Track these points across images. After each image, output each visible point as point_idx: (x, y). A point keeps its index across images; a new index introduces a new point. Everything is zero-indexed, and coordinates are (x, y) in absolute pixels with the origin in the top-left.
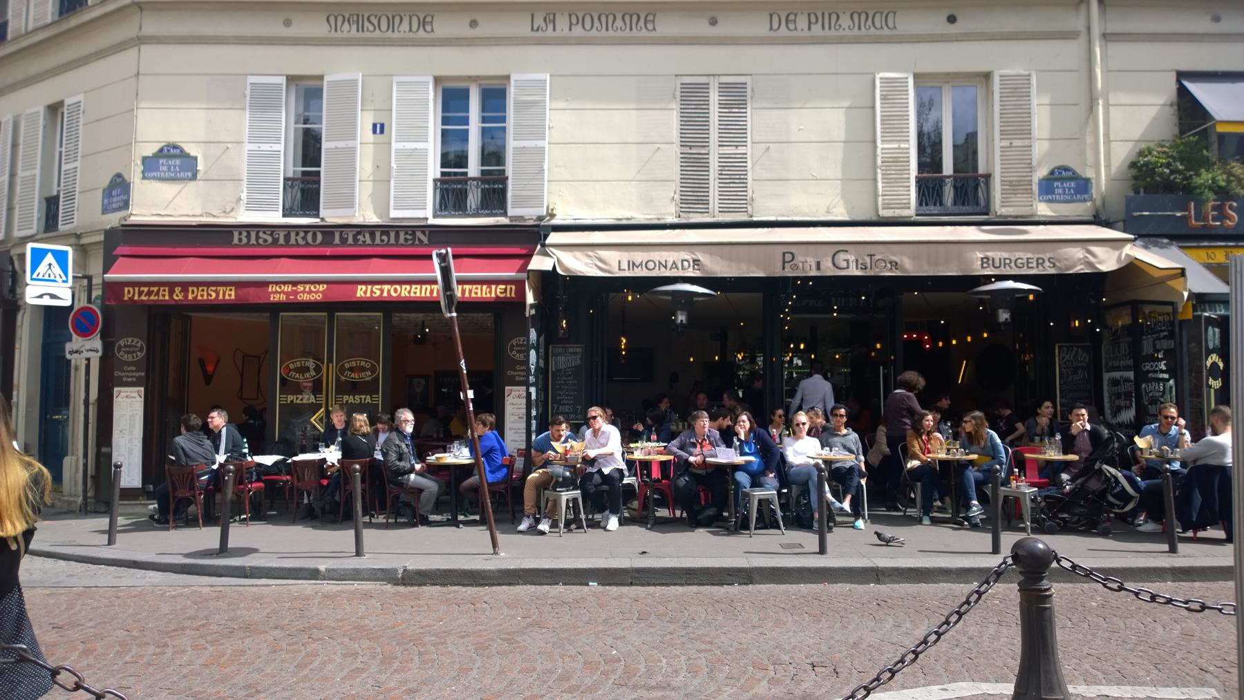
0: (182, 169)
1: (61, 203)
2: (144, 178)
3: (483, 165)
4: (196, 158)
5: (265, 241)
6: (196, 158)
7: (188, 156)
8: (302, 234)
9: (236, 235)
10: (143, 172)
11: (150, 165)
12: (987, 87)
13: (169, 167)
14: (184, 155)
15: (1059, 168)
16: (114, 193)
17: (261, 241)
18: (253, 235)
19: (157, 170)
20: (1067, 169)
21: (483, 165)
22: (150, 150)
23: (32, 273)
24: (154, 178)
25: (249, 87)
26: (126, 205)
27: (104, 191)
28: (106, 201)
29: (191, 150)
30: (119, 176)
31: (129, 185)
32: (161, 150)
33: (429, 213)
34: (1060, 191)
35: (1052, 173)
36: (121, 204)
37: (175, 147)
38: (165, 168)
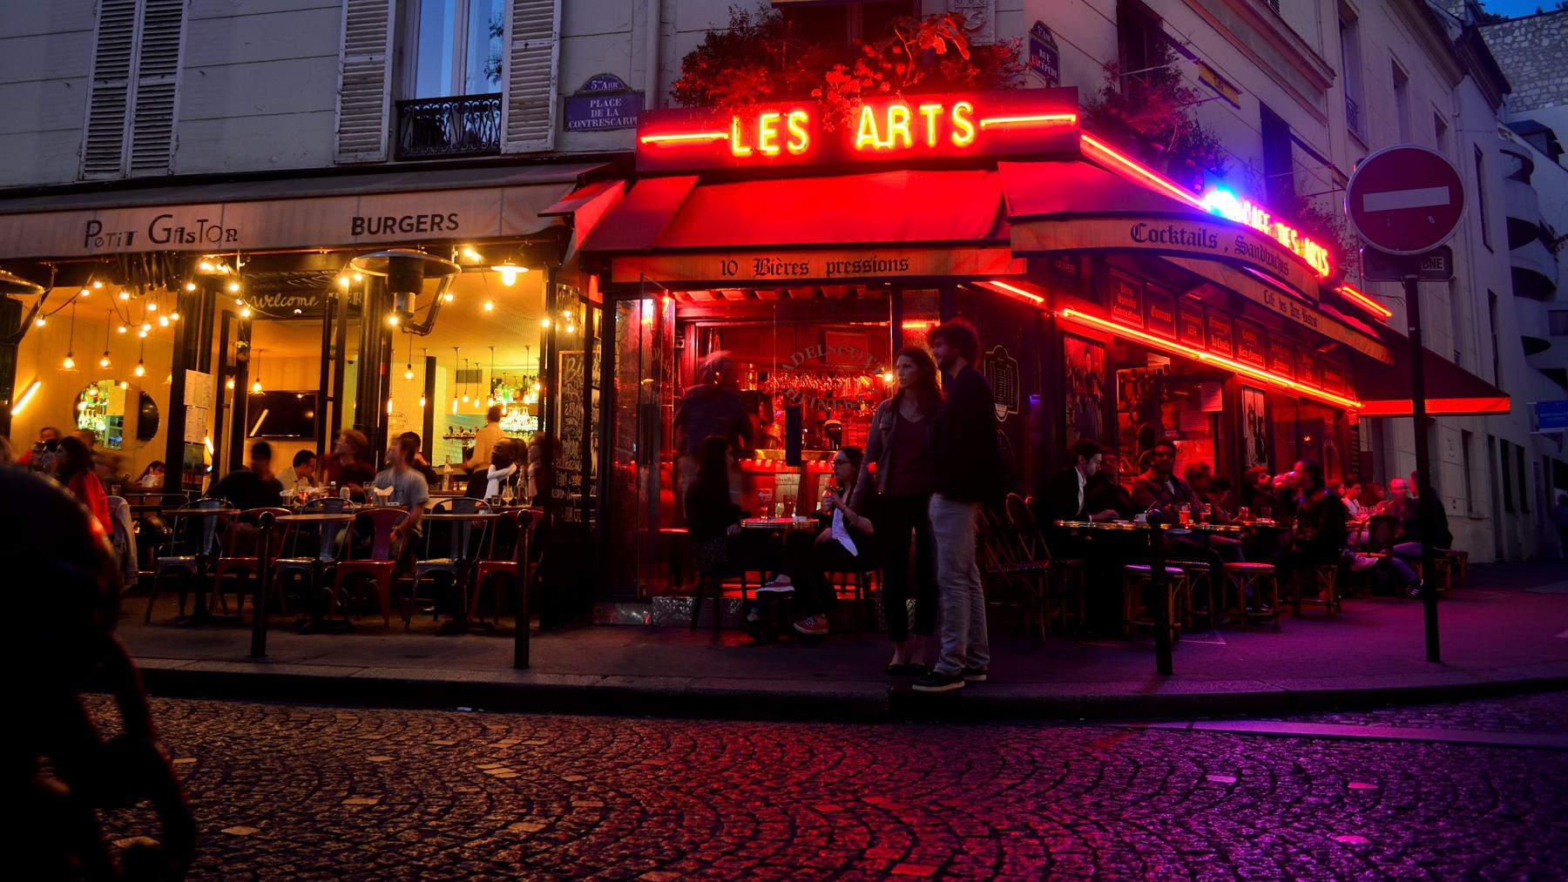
0: (624, 111)
13: (604, 109)
15: (598, 78)
19: (587, 116)
20: (609, 78)
34: (599, 113)
35: (588, 86)
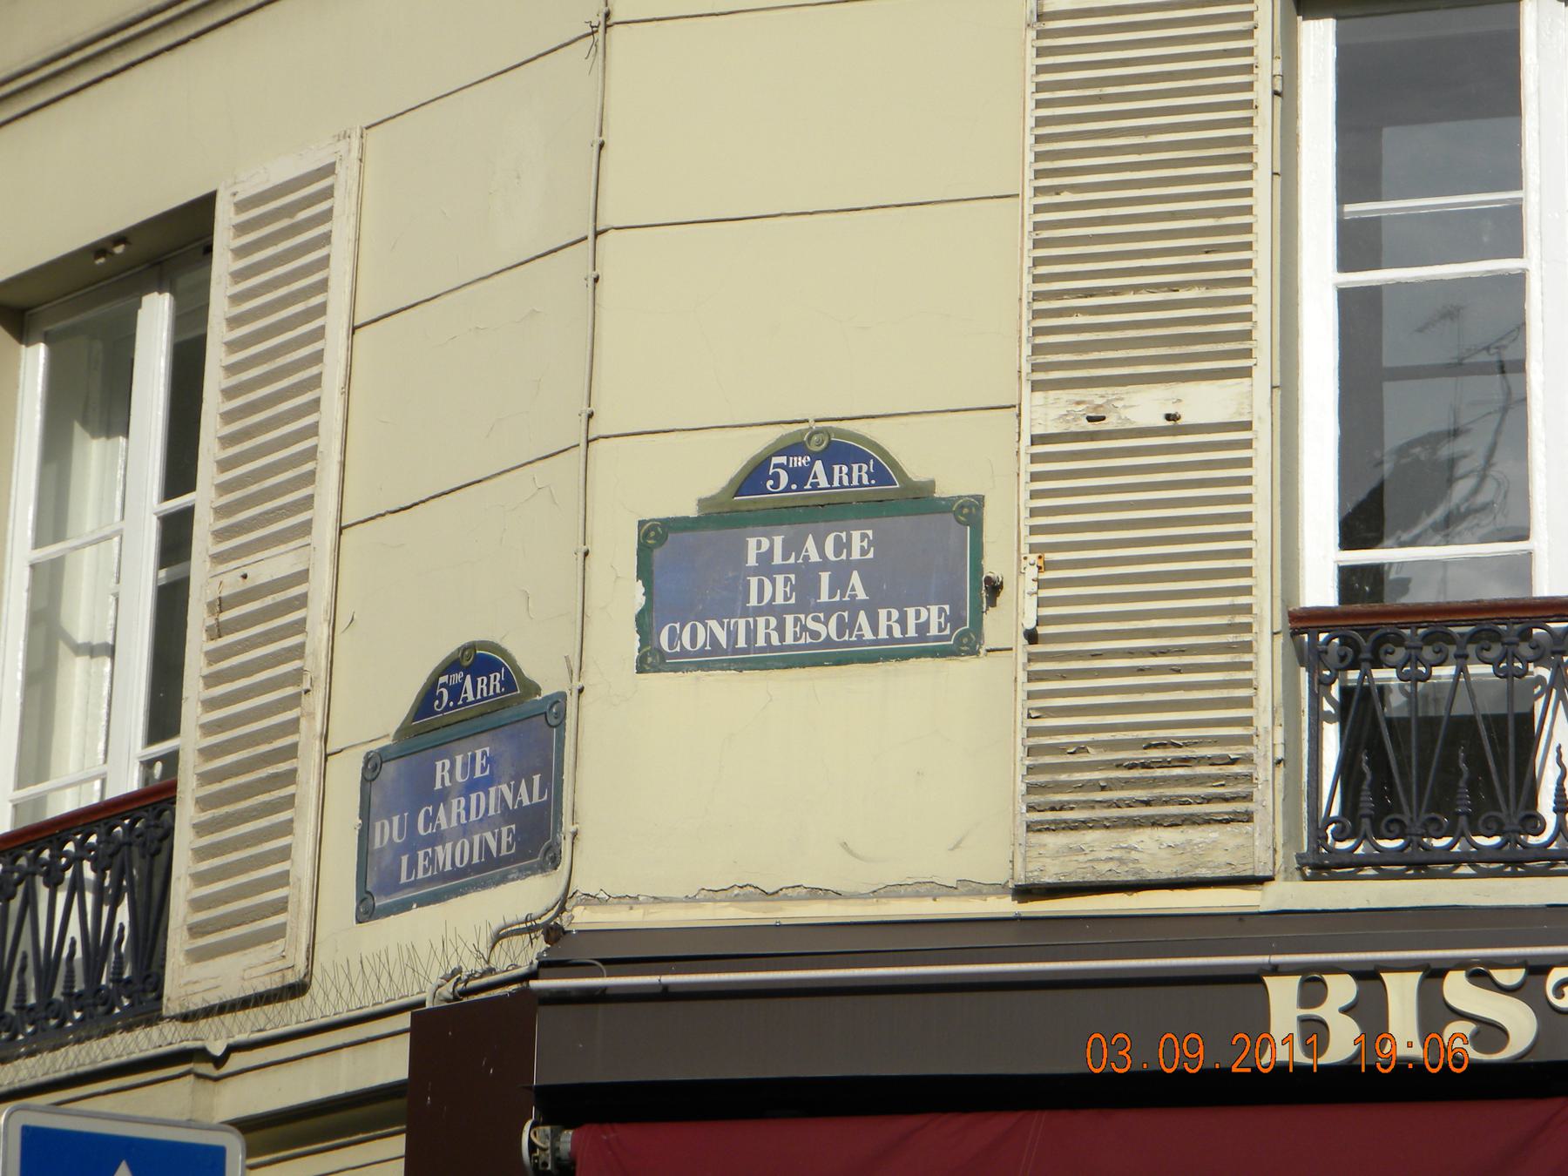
1: (184, 841)
4: (970, 512)
5: (1490, 1033)
6: (970, 512)
8: (1342, 989)
9: (1283, 994)
10: (645, 624)
11: (683, 565)
12: (29, 309)
14: (894, 498)
15: (451, 666)
16: (444, 773)
18: (1402, 991)
19: (731, 604)
22: (691, 478)
24: (712, 659)
26: (536, 839)
27: (373, 766)
28: (388, 832)
29: (929, 457)
30: (478, 661)
31: (553, 713)
32: (754, 477)
33: (1263, 840)
36: (501, 840)
37: (840, 451)
38: (779, 590)
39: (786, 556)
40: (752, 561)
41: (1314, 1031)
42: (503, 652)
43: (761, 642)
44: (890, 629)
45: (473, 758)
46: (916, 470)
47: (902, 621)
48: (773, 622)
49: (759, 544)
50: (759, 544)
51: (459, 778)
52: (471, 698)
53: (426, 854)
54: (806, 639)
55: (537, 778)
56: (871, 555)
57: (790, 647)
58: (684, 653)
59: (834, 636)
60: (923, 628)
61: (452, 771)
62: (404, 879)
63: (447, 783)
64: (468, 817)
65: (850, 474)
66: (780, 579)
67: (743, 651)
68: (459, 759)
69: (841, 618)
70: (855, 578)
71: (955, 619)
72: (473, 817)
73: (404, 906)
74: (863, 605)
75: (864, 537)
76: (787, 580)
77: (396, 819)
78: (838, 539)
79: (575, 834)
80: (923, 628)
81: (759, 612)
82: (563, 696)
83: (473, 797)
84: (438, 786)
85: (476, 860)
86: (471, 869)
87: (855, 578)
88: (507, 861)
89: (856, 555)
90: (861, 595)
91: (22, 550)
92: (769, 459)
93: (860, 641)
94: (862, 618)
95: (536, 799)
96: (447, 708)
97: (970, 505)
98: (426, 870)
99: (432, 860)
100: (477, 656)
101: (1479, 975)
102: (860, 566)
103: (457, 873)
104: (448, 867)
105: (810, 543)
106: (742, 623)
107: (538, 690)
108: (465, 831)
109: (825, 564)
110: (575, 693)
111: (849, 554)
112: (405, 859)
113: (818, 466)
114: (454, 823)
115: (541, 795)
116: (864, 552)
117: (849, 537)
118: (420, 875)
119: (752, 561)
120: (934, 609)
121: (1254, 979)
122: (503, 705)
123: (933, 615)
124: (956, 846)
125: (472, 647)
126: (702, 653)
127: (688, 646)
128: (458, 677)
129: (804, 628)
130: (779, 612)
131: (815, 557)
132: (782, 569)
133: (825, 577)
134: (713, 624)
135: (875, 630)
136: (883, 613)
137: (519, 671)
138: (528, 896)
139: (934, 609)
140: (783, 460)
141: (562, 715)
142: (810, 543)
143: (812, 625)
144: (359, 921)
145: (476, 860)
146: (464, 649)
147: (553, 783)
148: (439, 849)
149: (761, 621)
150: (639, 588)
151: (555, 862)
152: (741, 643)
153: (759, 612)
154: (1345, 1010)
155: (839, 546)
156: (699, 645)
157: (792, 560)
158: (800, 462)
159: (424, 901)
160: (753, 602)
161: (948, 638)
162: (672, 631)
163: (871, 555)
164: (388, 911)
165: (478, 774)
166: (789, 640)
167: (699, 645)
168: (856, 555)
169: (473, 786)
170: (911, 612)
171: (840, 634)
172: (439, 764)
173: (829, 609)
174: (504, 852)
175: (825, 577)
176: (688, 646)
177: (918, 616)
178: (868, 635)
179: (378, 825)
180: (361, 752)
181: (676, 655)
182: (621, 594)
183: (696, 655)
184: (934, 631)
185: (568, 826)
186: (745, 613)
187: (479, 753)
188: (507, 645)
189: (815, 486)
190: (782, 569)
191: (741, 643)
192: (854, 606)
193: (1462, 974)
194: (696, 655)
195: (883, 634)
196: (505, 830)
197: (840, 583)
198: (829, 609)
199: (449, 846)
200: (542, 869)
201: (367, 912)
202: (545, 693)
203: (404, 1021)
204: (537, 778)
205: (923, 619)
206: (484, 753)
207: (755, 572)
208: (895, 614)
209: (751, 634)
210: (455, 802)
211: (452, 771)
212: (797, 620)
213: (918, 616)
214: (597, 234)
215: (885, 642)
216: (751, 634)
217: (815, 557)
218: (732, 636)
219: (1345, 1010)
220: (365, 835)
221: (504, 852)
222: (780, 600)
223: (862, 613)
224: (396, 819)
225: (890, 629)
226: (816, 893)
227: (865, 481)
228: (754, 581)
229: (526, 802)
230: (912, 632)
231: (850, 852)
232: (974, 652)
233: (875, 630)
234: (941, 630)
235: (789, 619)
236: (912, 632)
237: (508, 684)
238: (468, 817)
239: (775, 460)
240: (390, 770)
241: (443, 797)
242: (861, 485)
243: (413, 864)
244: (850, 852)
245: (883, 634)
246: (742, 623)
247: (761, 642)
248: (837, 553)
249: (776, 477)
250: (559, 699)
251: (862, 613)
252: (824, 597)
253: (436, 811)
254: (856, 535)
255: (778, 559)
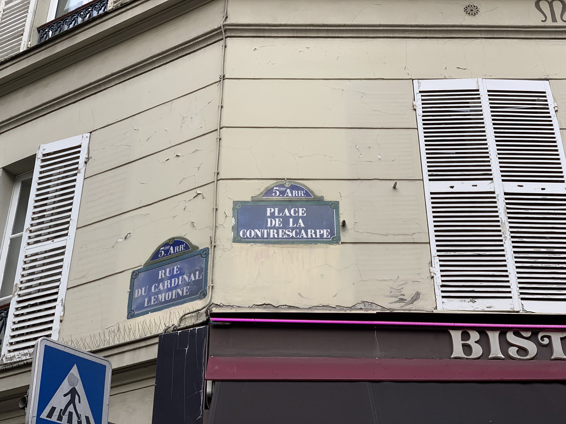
1: (11, 318)
2: (237, 239)
3: (462, 340)
5: (522, 350)
6: (335, 205)
7: (320, 200)
9: (456, 336)
10: (236, 229)
11: (249, 217)
13: (285, 221)
15: (165, 244)
17: (513, 351)
18: (494, 337)
19: (262, 225)
21: (462, 340)
23: (40, 410)
24: (256, 240)
25: (418, 97)
26: (199, 289)
27: (135, 275)
29: (326, 192)
38: (277, 223)
39: (279, 214)
40: (268, 214)
41: (467, 348)
42: (185, 239)
43: (272, 236)
44: (311, 235)
45: (173, 269)
46: (318, 194)
47: (315, 233)
48: (275, 231)
49: (271, 210)
50: (271, 210)
51: (168, 275)
52: (172, 252)
53: (155, 297)
54: (286, 236)
55: (197, 273)
56: (305, 215)
57: (281, 238)
58: (247, 238)
59: (294, 236)
60: (322, 236)
61: (165, 273)
62: (146, 305)
63: (163, 277)
64: (171, 285)
65: (298, 193)
66: (277, 220)
67: (266, 238)
68: (168, 270)
69: (296, 232)
70: (300, 221)
71: (332, 233)
72: (173, 285)
73: (147, 313)
74: (303, 228)
75: (303, 210)
76: (279, 220)
77: (143, 289)
78: (295, 210)
79: (212, 287)
80: (322, 236)
81: (271, 228)
82: (208, 248)
83: (173, 280)
84: (160, 277)
85: (174, 297)
86: (172, 300)
87: (300, 221)
88: (186, 296)
89: (300, 215)
90: (302, 225)
91: (8, 234)
92: (273, 188)
93: (302, 238)
94: (303, 231)
95: (197, 278)
96: (164, 256)
97: (335, 204)
98: (154, 302)
99: (157, 299)
100: (175, 241)
101: (517, 333)
102: (302, 218)
103: (166, 302)
104: (163, 300)
105: (286, 210)
106: (266, 231)
107: (198, 248)
108: (170, 289)
109: (291, 216)
110: (213, 247)
111: (298, 214)
112: (146, 300)
113: (288, 190)
114: (166, 287)
115: (199, 277)
116: (303, 214)
117: (298, 210)
118: (152, 303)
119: (268, 214)
120: (325, 231)
121: (445, 331)
122: (184, 253)
123: (325, 232)
124: (335, 296)
125: (173, 238)
126: (253, 238)
127: (248, 236)
128: (168, 247)
129: (285, 233)
130: (278, 229)
131: (288, 214)
132: (277, 217)
133: (291, 220)
134: (257, 230)
135: (307, 235)
136: (309, 231)
137: (191, 244)
138: (198, 304)
139: (325, 231)
140: (278, 188)
141: (207, 255)
142: (286, 210)
143: (287, 232)
144: (128, 319)
145: (174, 297)
146: (170, 239)
147: (204, 271)
148: (160, 296)
149: (272, 231)
150: (233, 220)
151: (205, 295)
152: (265, 236)
153: (271, 228)
154: (476, 342)
155: (295, 212)
156: (252, 236)
157: (281, 215)
158: (284, 189)
159: (153, 311)
160: (269, 225)
161: (330, 238)
162: (244, 232)
163: (305, 215)
164: (139, 315)
165: (175, 273)
166: (280, 236)
167: (252, 236)
168: (300, 215)
169: (172, 276)
170: (318, 231)
171: (296, 235)
172: (160, 272)
173: (293, 229)
174: (185, 294)
175: (291, 220)
176: (248, 236)
177: (320, 232)
178: (305, 236)
179: (137, 291)
180: (131, 271)
181: (245, 238)
182: (228, 222)
183: (251, 239)
184: (325, 236)
185: (209, 283)
186: (266, 228)
187: (175, 267)
188: (187, 237)
189: (287, 196)
190: (277, 217)
191: (265, 236)
192: (300, 228)
193: (512, 333)
194: (251, 239)
195: (309, 236)
196: (185, 288)
197: (296, 221)
198: (293, 229)
199: (163, 295)
200: (200, 298)
201: (131, 315)
202: (200, 249)
203: (157, 340)
204: (197, 273)
205: (322, 233)
206: (177, 267)
207: (269, 217)
208: (313, 231)
209: (268, 234)
210: (166, 282)
211: (165, 273)
212: (283, 231)
213: (320, 232)
214: (220, 128)
215: (310, 238)
216: (268, 234)
217: (288, 214)
218: (263, 234)
219: (476, 342)
220: (131, 294)
221: (185, 294)
222: (277, 225)
223: (303, 230)
224: (143, 289)
225: (311, 235)
226: (290, 307)
227: (303, 195)
228: (269, 220)
229: (193, 279)
230: (318, 236)
231: (301, 296)
232: (337, 243)
233: (307, 235)
234: (327, 236)
235: (280, 231)
236: (318, 236)
237: (187, 247)
238: (171, 285)
239: (275, 188)
240: (141, 275)
241: (162, 280)
242: (301, 196)
243: (149, 301)
244: (301, 296)
245: (309, 236)
246: (266, 231)
247: (272, 236)
248: (295, 214)
249: (276, 193)
250: (206, 250)
251: (303, 230)
252: (291, 225)
253: (159, 285)
254: (300, 209)
255: (276, 214)
